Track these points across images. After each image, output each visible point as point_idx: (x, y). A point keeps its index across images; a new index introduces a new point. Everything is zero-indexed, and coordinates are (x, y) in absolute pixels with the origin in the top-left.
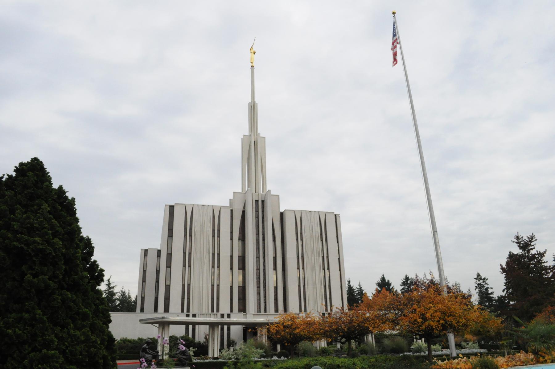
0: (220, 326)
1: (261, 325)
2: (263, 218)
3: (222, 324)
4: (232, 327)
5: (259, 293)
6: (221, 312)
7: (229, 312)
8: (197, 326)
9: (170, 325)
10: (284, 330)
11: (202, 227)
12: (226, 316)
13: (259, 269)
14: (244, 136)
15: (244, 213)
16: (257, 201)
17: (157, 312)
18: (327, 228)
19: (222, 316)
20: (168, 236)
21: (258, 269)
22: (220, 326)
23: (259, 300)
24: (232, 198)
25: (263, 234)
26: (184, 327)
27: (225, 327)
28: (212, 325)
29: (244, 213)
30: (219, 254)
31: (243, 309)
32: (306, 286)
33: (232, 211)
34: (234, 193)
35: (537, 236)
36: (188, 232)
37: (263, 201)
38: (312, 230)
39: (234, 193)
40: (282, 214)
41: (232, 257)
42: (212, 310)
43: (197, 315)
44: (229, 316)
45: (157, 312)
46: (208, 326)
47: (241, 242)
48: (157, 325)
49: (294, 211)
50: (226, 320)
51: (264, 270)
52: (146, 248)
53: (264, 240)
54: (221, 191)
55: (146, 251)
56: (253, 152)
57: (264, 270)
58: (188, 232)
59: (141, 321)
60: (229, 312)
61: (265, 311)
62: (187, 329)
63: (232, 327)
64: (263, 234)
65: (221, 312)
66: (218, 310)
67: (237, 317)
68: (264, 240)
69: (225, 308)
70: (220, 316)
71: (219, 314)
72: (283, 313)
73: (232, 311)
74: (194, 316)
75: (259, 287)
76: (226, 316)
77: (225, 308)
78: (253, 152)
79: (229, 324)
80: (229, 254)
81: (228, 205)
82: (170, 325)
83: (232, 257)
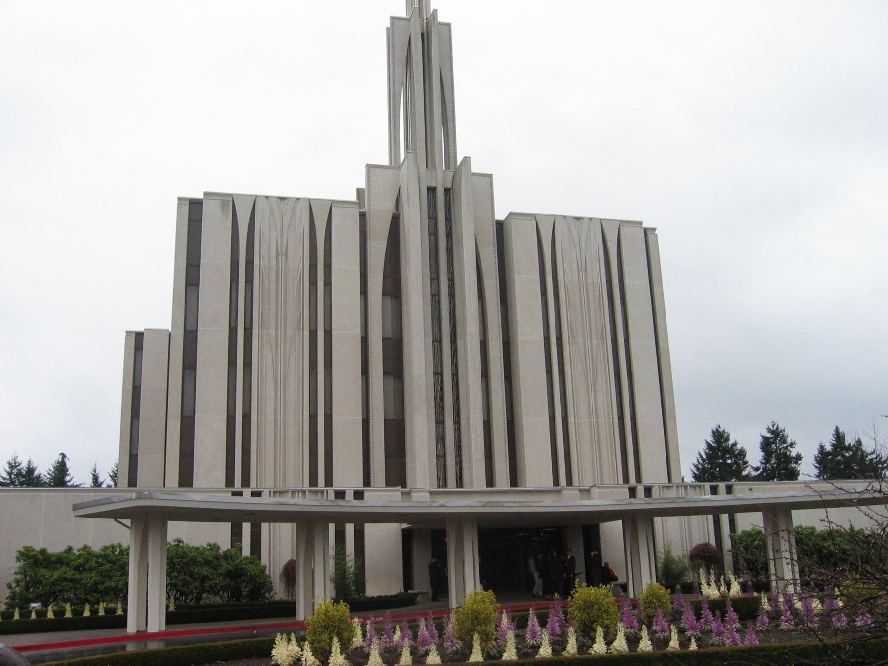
0: (332, 527)
1: (459, 519)
2: (449, 235)
3: (341, 519)
4: (370, 529)
5: (441, 438)
6: (338, 485)
7: (359, 485)
8: (265, 527)
9: (170, 524)
10: (843, 571)
11: (281, 260)
12: (350, 496)
13: (441, 374)
14: (393, 19)
15: (396, 220)
16: (432, 191)
17: (135, 486)
18: (623, 258)
19: (340, 495)
20: (188, 284)
21: (438, 374)
22: (332, 527)
23: (441, 457)
24: (362, 185)
25: (451, 280)
26: (225, 528)
27: (350, 529)
28: (309, 524)
29: (396, 220)
30: (328, 333)
31: (397, 476)
32: (571, 420)
33: (362, 215)
34: (369, 167)
35: (726, 427)
36: (242, 270)
37: (447, 191)
38: (583, 269)
39: (369, 167)
40: (500, 226)
41: (365, 340)
42: (313, 482)
43: (265, 494)
44: (359, 495)
45: (135, 486)
46: (759, 515)
47: (389, 300)
48: (128, 522)
49: (534, 215)
50: (350, 504)
51: (455, 375)
52: (140, 329)
53: (452, 295)
54: (327, 146)
55: (139, 336)
56: (421, 59)
57: (455, 375)
58: (242, 270)
59: (76, 507)
60: (359, 485)
61: (460, 482)
62: (236, 534)
63: (370, 529)
64: (451, 280)
65: (338, 485)
66: (329, 482)
67: (382, 497)
68: (452, 295)
69: (348, 476)
70: (332, 496)
71: (331, 492)
72: (507, 488)
73: (367, 482)
74: (257, 494)
75: (440, 422)
76: (350, 496)
77: (348, 476)
78: (421, 59)
79: (361, 519)
80: (357, 332)
81: (353, 198)
82: (170, 524)
83: (365, 340)
